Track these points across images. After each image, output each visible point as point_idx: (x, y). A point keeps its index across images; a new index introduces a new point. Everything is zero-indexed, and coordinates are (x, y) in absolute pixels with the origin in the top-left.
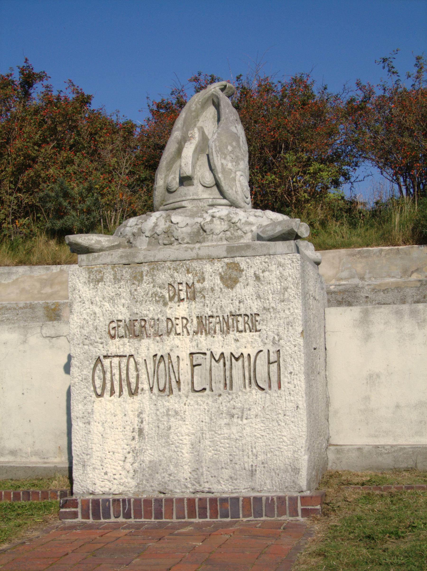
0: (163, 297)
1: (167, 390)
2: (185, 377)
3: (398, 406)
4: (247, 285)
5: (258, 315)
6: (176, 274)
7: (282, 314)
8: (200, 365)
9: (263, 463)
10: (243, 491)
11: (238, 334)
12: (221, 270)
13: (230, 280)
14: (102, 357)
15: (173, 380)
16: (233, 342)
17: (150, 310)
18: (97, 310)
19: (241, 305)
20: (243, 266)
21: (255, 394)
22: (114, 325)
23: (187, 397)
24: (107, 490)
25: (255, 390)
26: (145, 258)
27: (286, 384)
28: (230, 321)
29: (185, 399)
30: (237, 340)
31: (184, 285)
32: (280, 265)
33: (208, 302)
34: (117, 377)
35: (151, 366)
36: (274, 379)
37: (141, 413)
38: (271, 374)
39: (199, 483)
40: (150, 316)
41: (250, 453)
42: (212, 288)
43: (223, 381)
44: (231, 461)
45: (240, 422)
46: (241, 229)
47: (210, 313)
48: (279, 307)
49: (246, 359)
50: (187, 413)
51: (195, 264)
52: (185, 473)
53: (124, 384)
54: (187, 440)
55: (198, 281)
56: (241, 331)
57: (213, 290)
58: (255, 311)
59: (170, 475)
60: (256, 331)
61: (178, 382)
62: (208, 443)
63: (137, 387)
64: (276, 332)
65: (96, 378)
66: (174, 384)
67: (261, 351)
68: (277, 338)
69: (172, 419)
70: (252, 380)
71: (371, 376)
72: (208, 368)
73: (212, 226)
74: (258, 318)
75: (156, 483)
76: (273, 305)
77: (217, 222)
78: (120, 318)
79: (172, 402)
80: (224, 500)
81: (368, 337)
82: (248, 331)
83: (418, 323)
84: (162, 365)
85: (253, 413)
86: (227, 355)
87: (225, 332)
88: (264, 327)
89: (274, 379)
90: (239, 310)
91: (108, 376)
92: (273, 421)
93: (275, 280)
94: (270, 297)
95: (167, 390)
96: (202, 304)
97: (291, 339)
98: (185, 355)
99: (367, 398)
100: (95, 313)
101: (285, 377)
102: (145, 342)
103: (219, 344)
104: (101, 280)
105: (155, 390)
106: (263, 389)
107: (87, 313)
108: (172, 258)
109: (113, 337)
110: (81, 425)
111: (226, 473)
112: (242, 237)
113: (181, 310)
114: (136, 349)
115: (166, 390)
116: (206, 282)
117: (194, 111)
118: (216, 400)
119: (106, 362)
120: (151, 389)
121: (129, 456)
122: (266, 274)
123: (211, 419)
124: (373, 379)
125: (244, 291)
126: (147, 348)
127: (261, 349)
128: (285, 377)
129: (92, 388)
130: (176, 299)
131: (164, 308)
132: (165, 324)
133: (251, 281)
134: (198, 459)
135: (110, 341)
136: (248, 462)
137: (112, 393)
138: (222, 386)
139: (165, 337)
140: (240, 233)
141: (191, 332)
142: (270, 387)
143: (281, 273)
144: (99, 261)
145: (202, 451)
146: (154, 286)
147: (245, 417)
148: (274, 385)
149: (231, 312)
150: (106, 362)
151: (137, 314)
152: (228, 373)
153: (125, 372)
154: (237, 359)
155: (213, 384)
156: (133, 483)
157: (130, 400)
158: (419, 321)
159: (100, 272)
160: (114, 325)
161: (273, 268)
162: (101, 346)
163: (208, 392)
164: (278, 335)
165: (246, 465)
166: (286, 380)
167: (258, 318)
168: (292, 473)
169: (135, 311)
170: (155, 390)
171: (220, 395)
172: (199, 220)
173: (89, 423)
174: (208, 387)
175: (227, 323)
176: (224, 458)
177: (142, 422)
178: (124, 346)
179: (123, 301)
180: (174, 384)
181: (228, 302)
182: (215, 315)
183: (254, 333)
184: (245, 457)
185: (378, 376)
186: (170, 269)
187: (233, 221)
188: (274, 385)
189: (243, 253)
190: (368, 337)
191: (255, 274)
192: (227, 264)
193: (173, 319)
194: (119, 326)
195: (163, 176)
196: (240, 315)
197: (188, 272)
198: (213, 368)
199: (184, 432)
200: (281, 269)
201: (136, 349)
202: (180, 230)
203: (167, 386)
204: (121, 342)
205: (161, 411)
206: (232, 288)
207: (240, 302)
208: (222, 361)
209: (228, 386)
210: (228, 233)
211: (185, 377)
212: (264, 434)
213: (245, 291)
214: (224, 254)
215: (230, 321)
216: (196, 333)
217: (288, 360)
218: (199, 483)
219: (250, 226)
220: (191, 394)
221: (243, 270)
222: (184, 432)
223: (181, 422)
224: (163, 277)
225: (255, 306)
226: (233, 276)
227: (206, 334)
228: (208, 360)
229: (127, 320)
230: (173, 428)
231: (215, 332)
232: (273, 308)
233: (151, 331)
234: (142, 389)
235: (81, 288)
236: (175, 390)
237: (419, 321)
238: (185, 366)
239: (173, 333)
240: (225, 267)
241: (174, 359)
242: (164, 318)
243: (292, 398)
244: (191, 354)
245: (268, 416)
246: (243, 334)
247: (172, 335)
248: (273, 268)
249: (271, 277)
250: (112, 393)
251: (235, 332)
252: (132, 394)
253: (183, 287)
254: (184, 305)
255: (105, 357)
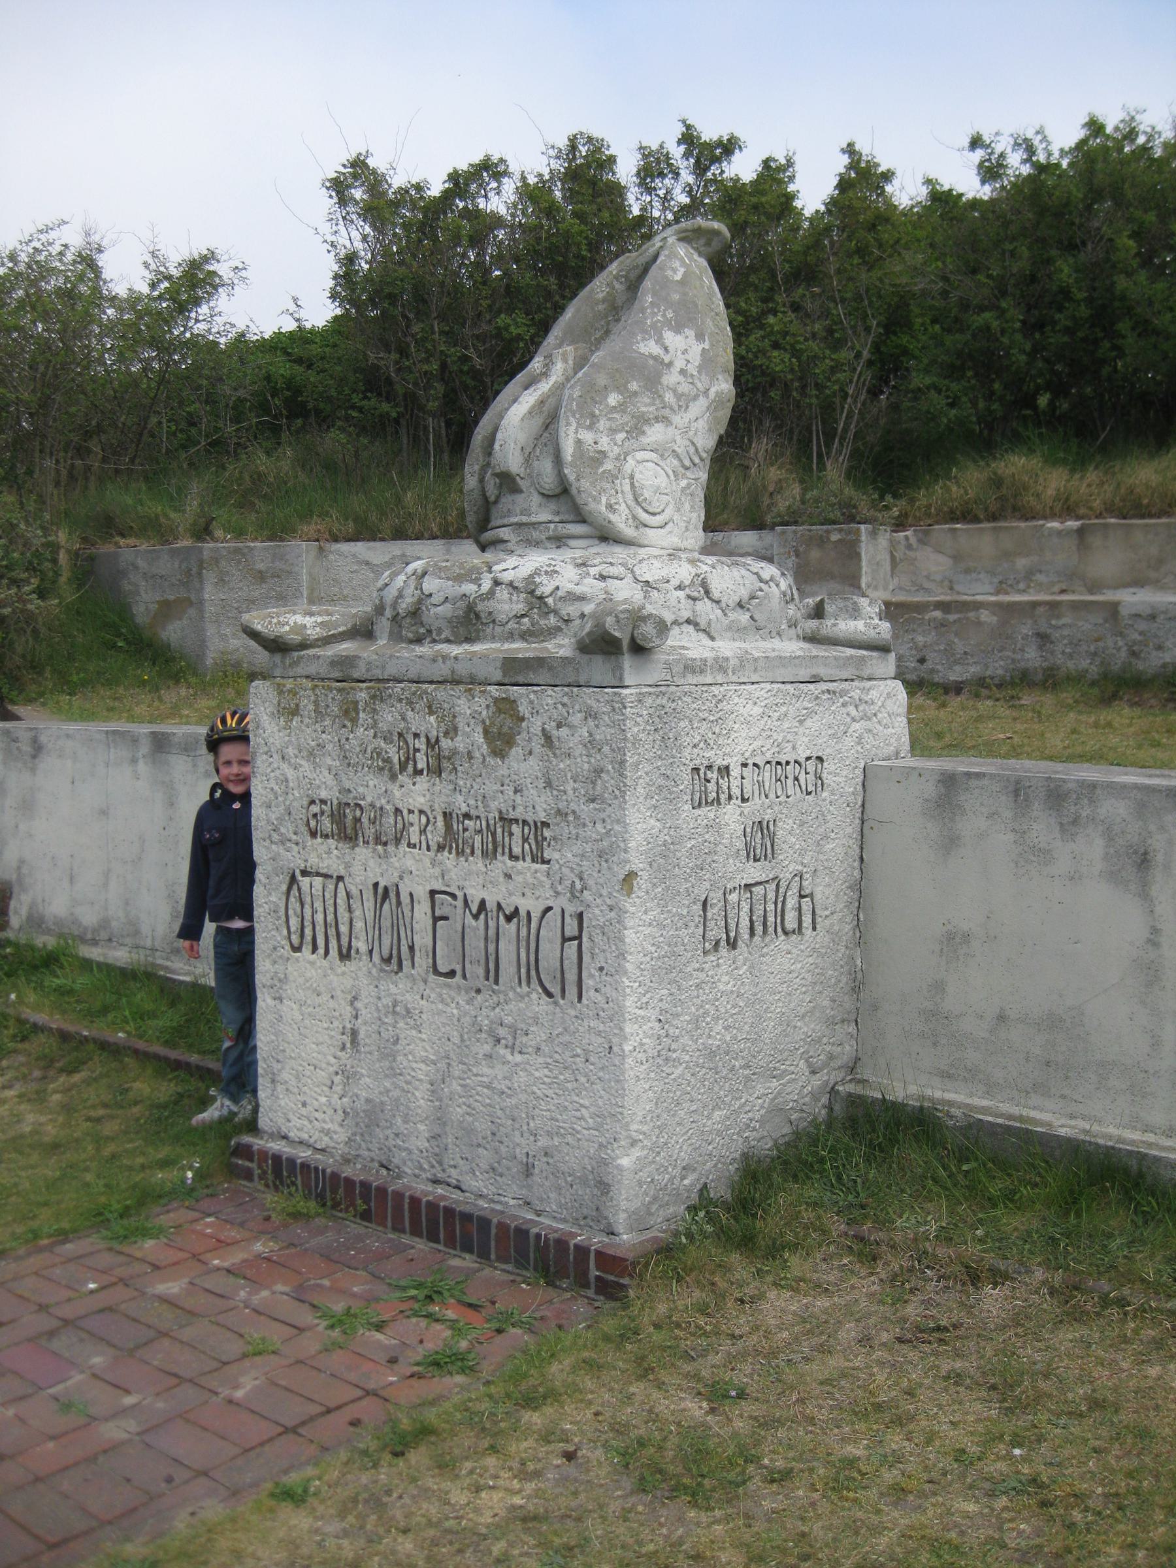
0: (388, 760)
1: (394, 960)
2: (422, 939)
3: (1002, 1018)
4: (530, 753)
5: (548, 825)
6: (410, 713)
7: (589, 832)
8: (445, 918)
9: (546, 1154)
10: (512, 1202)
11: (510, 863)
12: (484, 713)
13: (501, 741)
14: (298, 873)
15: (404, 942)
16: (501, 879)
17: (370, 788)
18: (290, 773)
19: (518, 798)
20: (524, 709)
21: (538, 1004)
22: (315, 809)
23: (425, 982)
24: (306, 1136)
25: (537, 994)
26: (368, 670)
27: (592, 993)
28: (499, 830)
29: (422, 985)
30: (508, 876)
31: (423, 739)
32: (590, 714)
33: (461, 783)
34: (319, 917)
35: (369, 904)
36: (571, 976)
37: (355, 998)
38: (566, 962)
39: (440, 1163)
40: (369, 799)
41: (525, 1128)
42: (469, 753)
43: (483, 961)
44: (494, 1134)
45: (510, 1058)
46: (555, 612)
47: (464, 809)
48: (585, 810)
49: (524, 921)
50: (424, 1016)
51: (442, 694)
52: (419, 1139)
53: (332, 932)
54: (422, 1071)
55: (446, 734)
56: (517, 858)
57: (470, 756)
58: (542, 816)
59: (397, 1135)
60: (543, 862)
61: (411, 948)
62: (455, 1086)
63: (350, 947)
64: (577, 869)
65: (291, 912)
66: (404, 949)
67: (549, 909)
68: (578, 886)
69: (401, 1024)
70: (531, 971)
71: (950, 937)
72: (460, 929)
73: (492, 605)
74: (547, 833)
75: (374, 1146)
76: (573, 806)
77: (502, 593)
78: (324, 794)
79: (399, 988)
80: (467, 1217)
81: (950, 843)
82: (528, 858)
83: (1061, 824)
84: (386, 906)
85: (530, 1041)
86: (491, 905)
87: (490, 854)
88: (556, 855)
89: (571, 976)
90: (514, 808)
91: (308, 911)
92: (566, 1068)
93: (579, 750)
94: (570, 786)
95: (394, 960)
96: (451, 787)
97: (604, 892)
98: (421, 893)
99: (938, 987)
100: (287, 781)
101: (592, 976)
102: (363, 853)
103: (477, 879)
104: (295, 712)
105: (376, 958)
106: (550, 995)
107: (276, 779)
108: (411, 676)
109: (313, 834)
110: (270, 1001)
111: (485, 1157)
112: (559, 629)
113: (417, 794)
114: (348, 866)
115: (394, 961)
116: (459, 738)
117: (604, 301)
118: (472, 999)
119: (305, 882)
120: (371, 952)
121: (337, 1079)
122: (564, 731)
123: (463, 1040)
124: (954, 942)
125: (523, 766)
126: (365, 866)
127: (550, 903)
128: (592, 976)
129: (285, 932)
130: (410, 769)
131: (390, 786)
132: (392, 821)
133: (537, 745)
134: (440, 1119)
135: (310, 842)
136: (523, 1145)
137: (315, 948)
138: (481, 971)
139: (391, 848)
140: (552, 620)
141: (434, 847)
142: (563, 991)
143: (591, 735)
144: (299, 670)
145: (446, 1101)
146: (375, 736)
147: (517, 1049)
148: (572, 991)
149: (500, 812)
150: (305, 882)
151: (349, 791)
152: (492, 948)
153: (332, 909)
154: (509, 919)
155: (468, 966)
156: (341, 1136)
157: (341, 968)
158: (1065, 820)
159: (295, 694)
160: (315, 809)
161: (577, 719)
162: (295, 848)
163: (458, 978)
164: (581, 879)
165: (518, 1151)
166: (591, 982)
167: (547, 833)
168: (596, 1191)
169: (347, 784)
170: (376, 958)
171: (478, 991)
172: (469, 588)
173: (281, 999)
174: (458, 968)
175: (494, 835)
176: (483, 1126)
177: (356, 1017)
178: (326, 854)
179: (329, 761)
180: (404, 949)
181: (495, 788)
182: (473, 813)
183: (538, 866)
184: (517, 1133)
185: (966, 938)
186: (400, 700)
187: (538, 593)
188: (572, 991)
189: (532, 677)
190: (950, 843)
191: (543, 730)
192: (496, 701)
193: (405, 812)
194: (322, 813)
195: (477, 468)
196: (517, 821)
197: (431, 713)
198: (467, 930)
199: (419, 1050)
200: (591, 723)
201: (348, 866)
202: (433, 610)
203: (395, 952)
204: (324, 848)
205: (385, 1001)
206: (503, 757)
207: (516, 792)
208: (482, 916)
209: (492, 974)
210: (526, 620)
211: (422, 939)
212: (550, 1092)
213: (523, 765)
214: (498, 676)
215: (499, 830)
216: (441, 848)
217: (598, 939)
218: (440, 1163)
219: (578, 605)
220: (432, 977)
221: (523, 719)
222: (419, 1050)
223: (414, 1032)
224: (388, 717)
225: (538, 804)
226: (505, 730)
227: (458, 853)
228: (460, 911)
229: (335, 802)
230: (402, 1042)
231: (473, 853)
232: (574, 812)
233: (370, 831)
234: (357, 951)
235: (266, 725)
236: (406, 963)
237: (1065, 820)
238: (422, 914)
239: (404, 843)
240: (493, 709)
241: (405, 898)
242: (389, 808)
243: (602, 1027)
244: (433, 893)
245: (557, 1056)
246: (520, 864)
247: (403, 847)
248: (577, 719)
249: (571, 740)
250: (315, 948)
251: (506, 858)
252: (345, 956)
253: (421, 744)
254: (423, 782)
255: (304, 873)
